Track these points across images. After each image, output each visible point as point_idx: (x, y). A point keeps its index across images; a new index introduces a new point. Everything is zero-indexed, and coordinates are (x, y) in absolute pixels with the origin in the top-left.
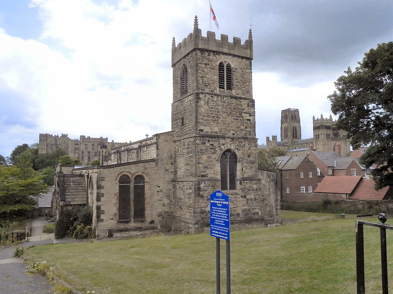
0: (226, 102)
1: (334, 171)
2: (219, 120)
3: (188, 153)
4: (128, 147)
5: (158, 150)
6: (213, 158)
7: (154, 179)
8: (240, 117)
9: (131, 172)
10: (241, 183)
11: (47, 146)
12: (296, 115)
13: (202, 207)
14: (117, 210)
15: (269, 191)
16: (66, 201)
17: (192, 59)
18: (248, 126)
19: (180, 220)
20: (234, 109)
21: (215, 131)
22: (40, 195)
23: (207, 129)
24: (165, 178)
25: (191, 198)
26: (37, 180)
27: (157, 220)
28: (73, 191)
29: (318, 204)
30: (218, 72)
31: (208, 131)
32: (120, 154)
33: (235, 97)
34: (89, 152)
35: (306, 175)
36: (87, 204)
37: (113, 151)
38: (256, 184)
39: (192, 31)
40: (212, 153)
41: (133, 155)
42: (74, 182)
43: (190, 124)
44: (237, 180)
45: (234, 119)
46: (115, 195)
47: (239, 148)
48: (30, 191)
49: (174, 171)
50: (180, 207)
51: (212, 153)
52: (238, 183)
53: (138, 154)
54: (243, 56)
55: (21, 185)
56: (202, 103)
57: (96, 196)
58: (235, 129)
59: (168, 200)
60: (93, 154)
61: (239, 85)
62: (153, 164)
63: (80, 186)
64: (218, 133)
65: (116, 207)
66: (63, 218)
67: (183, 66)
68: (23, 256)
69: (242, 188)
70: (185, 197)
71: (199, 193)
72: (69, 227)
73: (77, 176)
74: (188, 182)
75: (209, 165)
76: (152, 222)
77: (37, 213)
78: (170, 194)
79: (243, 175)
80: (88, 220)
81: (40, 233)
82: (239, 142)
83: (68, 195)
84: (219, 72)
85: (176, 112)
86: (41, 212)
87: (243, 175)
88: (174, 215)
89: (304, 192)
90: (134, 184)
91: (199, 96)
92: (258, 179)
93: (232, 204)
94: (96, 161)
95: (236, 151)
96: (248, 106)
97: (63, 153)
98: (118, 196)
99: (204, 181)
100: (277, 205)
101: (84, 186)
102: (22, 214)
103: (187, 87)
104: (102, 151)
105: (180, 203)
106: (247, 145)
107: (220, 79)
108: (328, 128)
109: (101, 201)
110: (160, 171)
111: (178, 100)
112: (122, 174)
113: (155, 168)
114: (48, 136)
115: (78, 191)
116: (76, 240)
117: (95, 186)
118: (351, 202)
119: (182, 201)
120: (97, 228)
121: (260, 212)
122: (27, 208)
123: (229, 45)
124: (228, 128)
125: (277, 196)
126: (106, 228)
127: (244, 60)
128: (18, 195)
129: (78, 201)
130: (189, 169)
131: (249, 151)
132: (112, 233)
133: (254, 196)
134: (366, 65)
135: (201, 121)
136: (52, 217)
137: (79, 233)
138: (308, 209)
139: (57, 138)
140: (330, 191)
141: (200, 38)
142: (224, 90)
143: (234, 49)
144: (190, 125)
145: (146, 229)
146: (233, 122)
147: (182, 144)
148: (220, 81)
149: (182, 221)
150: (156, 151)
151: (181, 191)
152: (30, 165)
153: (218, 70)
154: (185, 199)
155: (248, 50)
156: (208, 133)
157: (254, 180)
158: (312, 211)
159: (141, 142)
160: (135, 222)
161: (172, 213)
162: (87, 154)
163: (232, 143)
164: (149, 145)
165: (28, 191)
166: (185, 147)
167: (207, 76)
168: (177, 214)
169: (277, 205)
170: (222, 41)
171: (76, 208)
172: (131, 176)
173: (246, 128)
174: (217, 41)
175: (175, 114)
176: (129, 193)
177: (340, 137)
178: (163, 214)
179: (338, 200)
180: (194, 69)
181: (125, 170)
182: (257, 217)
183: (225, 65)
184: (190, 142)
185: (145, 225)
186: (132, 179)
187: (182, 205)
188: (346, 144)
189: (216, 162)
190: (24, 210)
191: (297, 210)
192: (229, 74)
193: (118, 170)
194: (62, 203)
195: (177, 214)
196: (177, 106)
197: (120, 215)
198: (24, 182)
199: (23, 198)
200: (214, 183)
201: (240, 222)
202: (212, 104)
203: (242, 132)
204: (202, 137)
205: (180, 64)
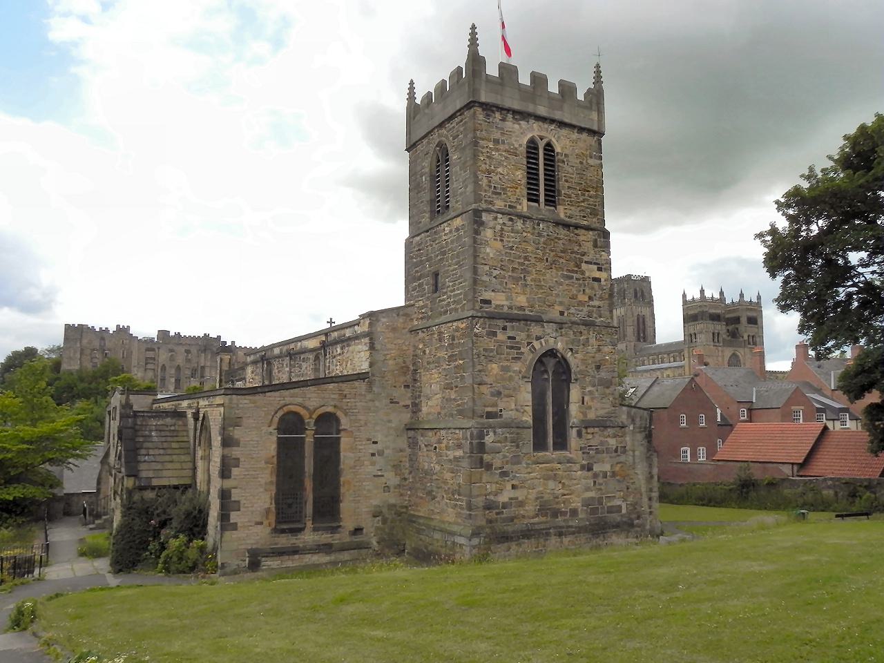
2: (529, 279)
3: (452, 358)
4: (292, 346)
5: (373, 352)
6: (514, 372)
7: (362, 423)
9: (307, 403)
10: (579, 434)
11: (81, 354)
12: (644, 290)
13: (489, 494)
14: (271, 500)
15: (634, 456)
16: (141, 476)
17: (462, 129)
18: (595, 295)
19: (429, 527)
21: (518, 304)
22: (70, 463)
23: (499, 300)
24: (390, 421)
25: (458, 471)
26: (62, 426)
27: (371, 527)
28: (157, 452)
29: (725, 487)
31: (502, 303)
32: (269, 364)
33: (565, 223)
34: (178, 368)
35: (693, 421)
36: (193, 485)
37: (249, 359)
38: (615, 436)
39: (461, 60)
40: (513, 358)
41: (304, 365)
42: (160, 431)
43: (456, 288)
44: (572, 427)
46: (266, 463)
48: (46, 453)
49: (412, 403)
50: (430, 493)
51: (513, 358)
52: (573, 432)
53: (317, 362)
54: (583, 126)
55: (23, 438)
56: (488, 233)
57: (218, 464)
58: (566, 301)
59: (396, 475)
60: (188, 372)
62: (361, 386)
63: (175, 439)
64: (524, 310)
65: (270, 493)
66: (133, 519)
67: (437, 146)
68: (34, 627)
69: (583, 446)
71: (482, 458)
72: (147, 543)
73: (166, 414)
74: (454, 431)
75: (504, 387)
76: (358, 531)
77: (61, 506)
78: (401, 462)
79: (585, 414)
80: (195, 525)
81: (71, 560)
82: (574, 333)
83: (145, 461)
84: (528, 162)
85: (419, 259)
86: (68, 504)
87: (585, 414)
88: (412, 512)
89: (689, 461)
90: (314, 434)
92: (621, 425)
93: (560, 486)
94: (195, 388)
95: (569, 355)
96: (595, 246)
97: (118, 370)
98: (275, 466)
99: (494, 427)
100: (651, 490)
101: (185, 439)
102: (23, 509)
103: (448, 197)
104: (221, 360)
105: (429, 484)
106: (593, 341)
107: (528, 178)
108: (715, 318)
109: (233, 477)
110: (377, 403)
111: (425, 229)
112: (286, 409)
113: (365, 395)
114: (84, 330)
115: (169, 452)
116: (165, 575)
117: (217, 440)
118: (805, 483)
119: (435, 477)
120: (221, 547)
121: (624, 507)
122: (36, 494)
124: (549, 298)
125: (650, 466)
126: (243, 547)
127: (584, 136)
128: (16, 463)
129: (170, 477)
130: (453, 397)
131: (598, 357)
132: (259, 558)
133: (612, 466)
134: (845, 162)
135: (485, 278)
136: (98, 516)
137: (175, 559)
138: (702, 499)
139: (105, 335)
140: (753, 457)
141: (484, 77)
142: (539, 205)
143: (561, 108)
145: (343, 548)
146: (561, 284)
147: (436, 336)
149: (434, 529)
150: (368, 354)
151: (432, 454)
152: (46, 390)
153: (525, 156)
154: (442, 473)
155: (594, 112)
156: (502, 309)
157: (609, 427)
158: (712, 504)
159: (326, 335)
160: (315, 530)
161: (406, 507)
162: (173, 371)
164: (349, 339)
165: (41, 454)
166: (443, 344)
167: (500, 170)
168: (419, 511)
169: (651, 490)
170: (534, 88)
171: (165, 494)
172: (308, 416)
174: (521, 86)
175: (416, 265)
176: (303, 457)
177: (741, 339)
178: (385, 510)
179: (774, 479)
180: (469, 152)
181: (294, 401)
182: (616, 517)
184: (457, 330)
185: (340, 539)
186: (310, 422)
187: (434, 489)
189: (521, 382)
190: (29, 499)
191: (676, 501)
192: (550, 168)
193: (275, 398)
194: (129, 483)
195: (419, 511)
196: (419, 245)
197: (278, 514)
198: (30, 432)
199: (27, 470)
200: (518, 434)
201: (580, 530)
204: (489, 318)
205: (429, 143)
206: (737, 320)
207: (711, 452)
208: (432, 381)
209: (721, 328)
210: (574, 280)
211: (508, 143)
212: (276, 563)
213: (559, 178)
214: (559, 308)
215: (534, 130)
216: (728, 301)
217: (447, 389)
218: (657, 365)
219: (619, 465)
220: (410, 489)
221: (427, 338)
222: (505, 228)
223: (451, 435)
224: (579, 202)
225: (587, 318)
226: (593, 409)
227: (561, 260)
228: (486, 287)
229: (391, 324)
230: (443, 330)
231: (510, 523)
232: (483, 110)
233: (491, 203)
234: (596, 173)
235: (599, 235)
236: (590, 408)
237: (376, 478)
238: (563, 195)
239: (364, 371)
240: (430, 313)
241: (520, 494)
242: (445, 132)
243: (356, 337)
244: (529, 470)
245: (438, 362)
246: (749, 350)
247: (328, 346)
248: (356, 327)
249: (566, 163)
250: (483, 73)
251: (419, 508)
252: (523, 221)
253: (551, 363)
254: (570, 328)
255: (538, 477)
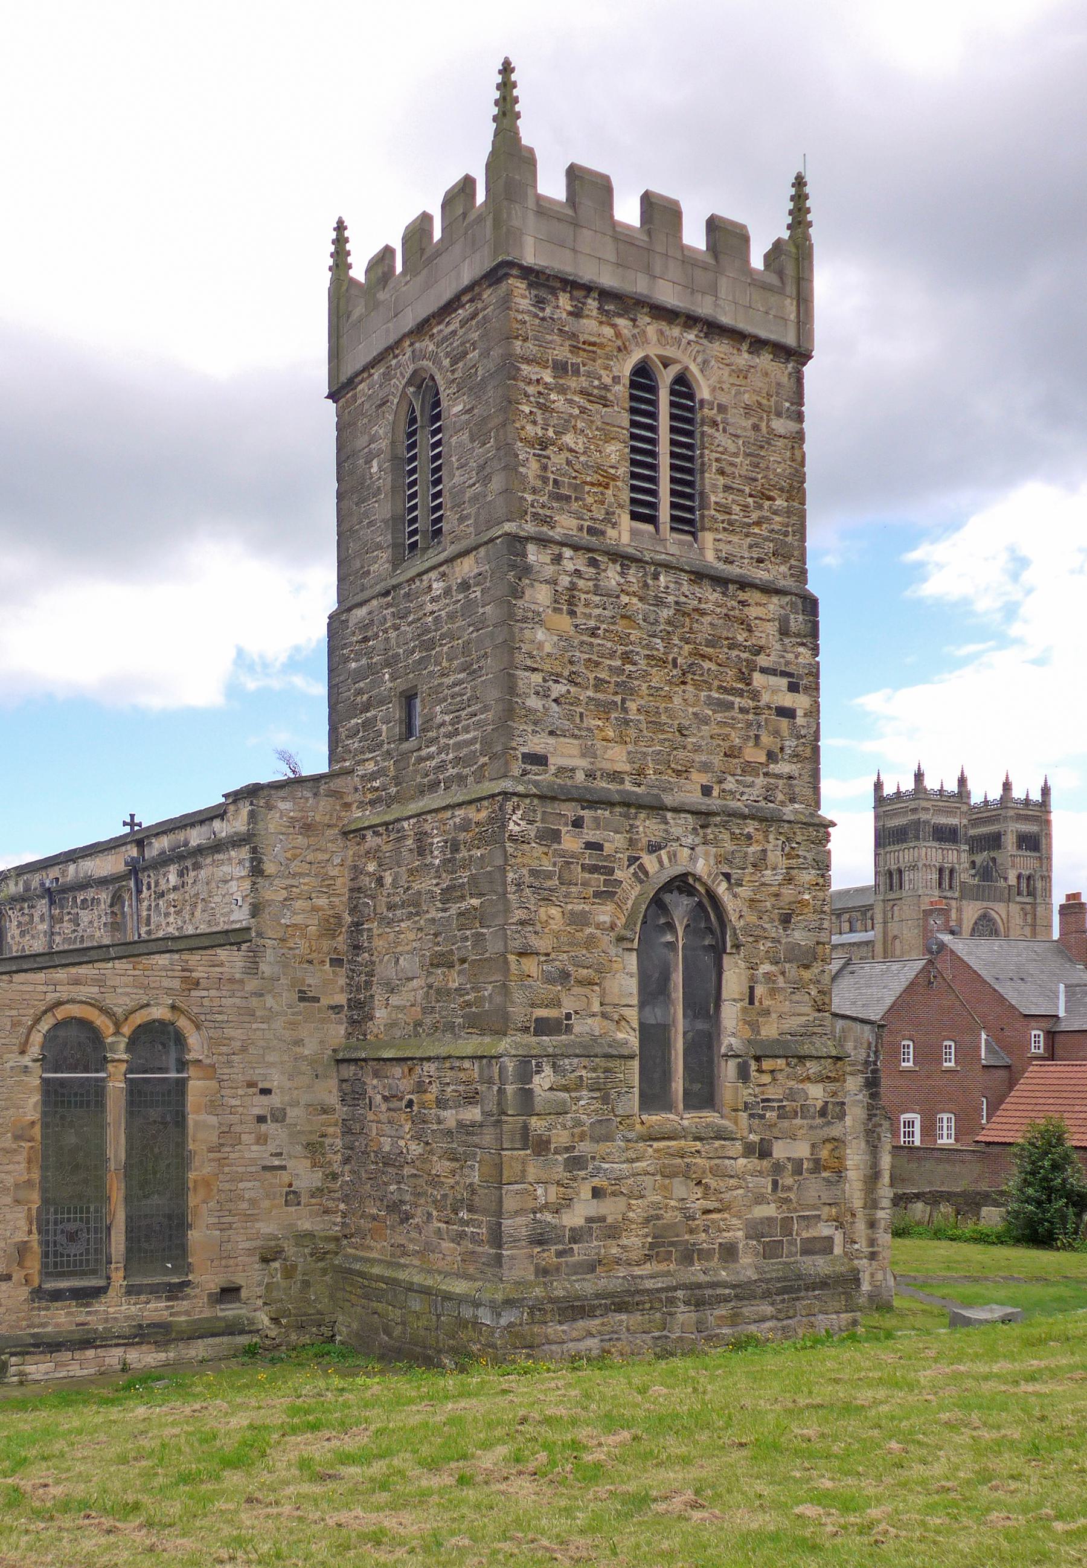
0: (671, 599)
1: (1059, 1039)
2: (632, 706)
3: (449, 894)
4: (54, 872)
5: (259, 880)
8: (740, 693)
9: (110, 1000)
10: (743, 1074)
14: (31, 1224)
17: (475, 336)
20: (710, 644)
21: (608, 766)
24: (299, 1042)
25: (468, 1157)
30: (625, 419)
35: (928, 1055)
40: (597, 894)
41: (85, 916)
45: (710, 702)
47: (736, 873)
52: (729, 1070)
53: (116, 909)
54: (763, 334)
56: (540, 596)
61: (736, 508)
62: (231, 960)
64: (622, 782)
67: (409, 383)
70: (431, 1152)
71: (525, 1127)
76: (229, 1293)
84: (634, 424)
85: (364, 661)
87: (754, 1027)
89: (917, 1143)
91: (524, 555)
95: (721, 888)
103: (439, 507)
105: (393, 1187)
106: (774, 856)
108: (946, 835)
110: (270, 1001)
112: (61, 1013)
123: (687, 258)
127: (765, 360)
133: (813, 1146)
135: (534, 702)
141: (531, 203)
144: (466, 730)
146: (706, 721)
148: (634, 476)
150: (247, 885)
157: (811, 1057)
160: (131, 1291)
161: (337, 1239)
163: (698, 840)
164: (200, 850)
167: (568, 439)
168: (370, 1248)
172: (112, 1030)
173: (771, 756)
174: (618, 229)
177: (1002, 883)
183: (665, 378)
185: (187, 1313)
187: (407, 1198)
188: (1029, 918)
195: (370, 1248)
200: (607, 1070)
202: (591, 611)
203: (749, 779)
204: (542, 797)
205: (387, 376)
206: (995, 841)
207: (965, 1126)
208: (400, 949)
209: (957, 857)
210: (735, 713)
211: (588, 374)
212: (43, 1367)
213: (703, 464)
214: (700, 778)
215: (652, 341)
216: (976, 799)
217: (438, 966)
218: (861, 934)
219: (829, 1146)
220: (345, 1199)
221: (389, 847)
222: (581, 583)
223: (450, 1073)
224: (749, 525)
225: (763, 804)
226: (774, 1016)
227: (707, 665)
228: (535, 723)
229: (300, 815)
230: (427, 827)
231: (588, 1276)
232: (530, 286)
233: (547, 521)
234: (788, 453)
235: (793, 604)
236: (767, 1012)
237: (268, 1175)
238: (713, 506)
239: (238, 926)
240: (393, 790)
241: (611, 1209)
242: (431, 347)
243: (217, 847)
244: (631, 1154)
245: (415, 904)
246: (1018, 907)
247: (145, 869)
248: (217, 824)
249: (721, 427)
250: (530, 191)
251: (368, 1241)
252: (622, 565)
253: (680, 908)
254: (724, 825)
255: (651, 1169)
